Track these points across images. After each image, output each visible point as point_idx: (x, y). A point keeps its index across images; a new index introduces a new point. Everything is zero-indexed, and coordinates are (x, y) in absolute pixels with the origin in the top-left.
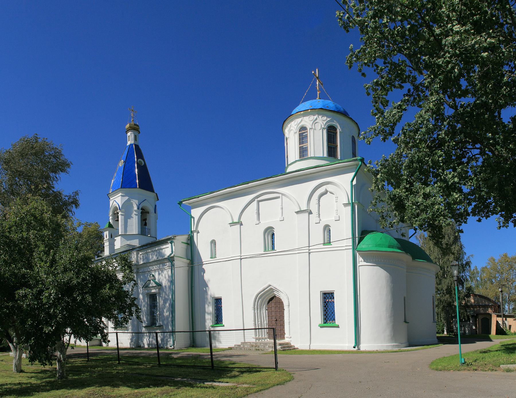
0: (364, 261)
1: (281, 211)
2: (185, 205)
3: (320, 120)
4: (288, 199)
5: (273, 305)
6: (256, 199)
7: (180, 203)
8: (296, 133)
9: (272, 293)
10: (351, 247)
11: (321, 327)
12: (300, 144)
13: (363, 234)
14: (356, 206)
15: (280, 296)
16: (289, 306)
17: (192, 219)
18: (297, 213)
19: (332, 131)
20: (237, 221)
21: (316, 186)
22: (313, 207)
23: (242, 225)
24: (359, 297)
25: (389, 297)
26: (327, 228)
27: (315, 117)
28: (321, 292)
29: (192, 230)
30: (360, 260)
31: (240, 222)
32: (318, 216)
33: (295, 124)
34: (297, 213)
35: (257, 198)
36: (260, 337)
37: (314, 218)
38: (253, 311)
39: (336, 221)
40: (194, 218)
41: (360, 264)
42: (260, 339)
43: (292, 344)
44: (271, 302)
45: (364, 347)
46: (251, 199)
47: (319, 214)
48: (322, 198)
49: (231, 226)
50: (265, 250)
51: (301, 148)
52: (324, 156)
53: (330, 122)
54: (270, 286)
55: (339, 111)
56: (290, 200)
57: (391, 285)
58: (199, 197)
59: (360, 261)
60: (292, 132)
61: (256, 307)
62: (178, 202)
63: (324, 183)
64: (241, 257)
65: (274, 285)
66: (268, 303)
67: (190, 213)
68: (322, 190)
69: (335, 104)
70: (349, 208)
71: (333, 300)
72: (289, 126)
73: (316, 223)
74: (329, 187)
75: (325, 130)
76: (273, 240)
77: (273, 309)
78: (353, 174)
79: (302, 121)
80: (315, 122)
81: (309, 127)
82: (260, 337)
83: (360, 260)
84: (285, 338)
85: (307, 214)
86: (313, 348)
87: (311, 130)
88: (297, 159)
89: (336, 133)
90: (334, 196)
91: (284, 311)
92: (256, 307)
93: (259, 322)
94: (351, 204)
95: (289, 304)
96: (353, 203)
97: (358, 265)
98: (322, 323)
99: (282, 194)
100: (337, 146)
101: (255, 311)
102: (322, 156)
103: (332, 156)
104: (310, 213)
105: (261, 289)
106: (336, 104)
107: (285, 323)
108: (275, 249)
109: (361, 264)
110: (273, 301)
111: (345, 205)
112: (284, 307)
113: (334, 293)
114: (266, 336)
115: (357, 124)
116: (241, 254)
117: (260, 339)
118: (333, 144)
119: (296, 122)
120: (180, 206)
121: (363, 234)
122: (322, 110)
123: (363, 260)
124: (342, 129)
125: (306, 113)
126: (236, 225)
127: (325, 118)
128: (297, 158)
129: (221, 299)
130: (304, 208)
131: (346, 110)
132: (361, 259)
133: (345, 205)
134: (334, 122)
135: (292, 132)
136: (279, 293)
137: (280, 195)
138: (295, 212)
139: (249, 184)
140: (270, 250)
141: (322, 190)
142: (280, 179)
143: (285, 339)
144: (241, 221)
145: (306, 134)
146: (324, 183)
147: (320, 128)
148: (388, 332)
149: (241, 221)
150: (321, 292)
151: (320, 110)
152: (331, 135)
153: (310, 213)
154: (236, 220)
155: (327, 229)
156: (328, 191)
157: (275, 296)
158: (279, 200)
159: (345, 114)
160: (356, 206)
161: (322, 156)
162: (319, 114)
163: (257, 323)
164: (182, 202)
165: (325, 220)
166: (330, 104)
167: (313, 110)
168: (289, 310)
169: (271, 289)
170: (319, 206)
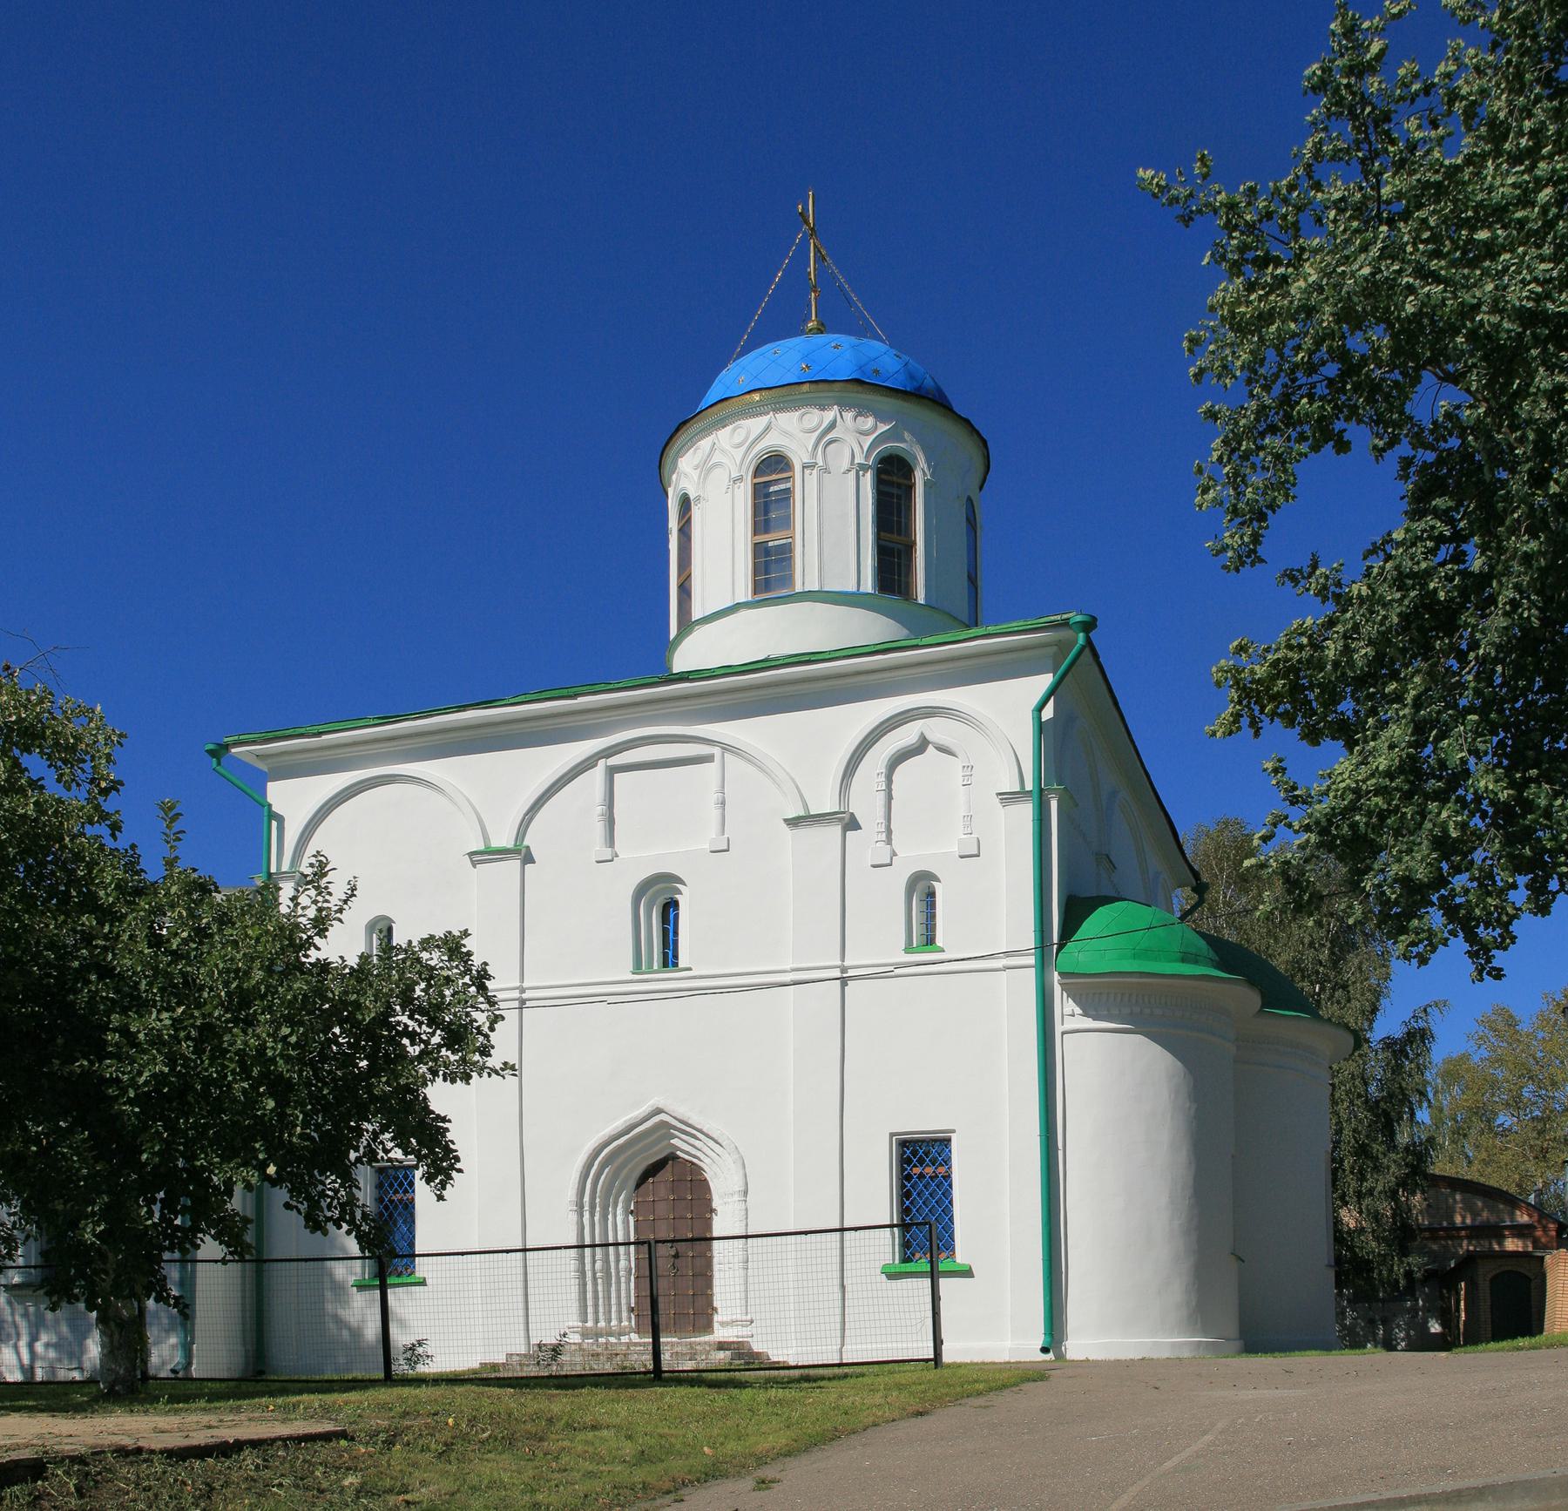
0: (1086, 1014)
1: (715, 813)
2: (238, 762)
3: (847, 429)
4: (751, 768)
5: (662, 1191)
6: (602, 762)
7: (220, 751)
8: (740, 479)
9: (664, 1143)
10: (1031, 960)
11: (892, 1276)
12: (755, 532)
13: (1076, 911)
14: (1054, 804)
15: (698, 1154)
16: (746, 1193)
17: (274, 824)
18: (793, 822)
19: (895, 479)
20: (510, 845)
21: (882, 723)
22: (865, 800)
23: (534, 862)
24: (1060, 1153)
25: (1183, 1156)
26: (921, 886)
27: (830, 415)
28: (892, 1135)
29: (273, 870)
30: (1067, 1010)
31: (524, 850)
32: (884, 837)
33: (738, 439)
34: (793, 822)
35: (608, 757)
36: (602, 1324)
37: (865, 845)
38: (574, 1217)
39: (962, 857)
40: (280, 820)
41: (1067, 1027)
42: (598, 1335)
43: (756, 1348)
44: (651, 1180)
45: (1078, 1346)
46: (579, 760)
47: (889, 832)
48: (901, 769)
49: (474, 864)
50: (637, 967)
51: (760, 551)
52: (862, 590)
53: (885, 442)
54: (659, 1111)
55: (919, 388)
56: (763, 770)
57: (1190, 1108)
58: (320, 734)
59: (1067, 1012)
60: (720, 478)
61: (586, 1199)
62: (210, 747)
63: (911, 714)
64: (523, 991)
65: (681, 1108)
66: (638, 1186)
67: (264, 794)
68: (905, 736)
69: (904, 356)
70: (1026, 811)
71: (942, 1170)
72: (705, 444)
73: (874, 866)
74: (935, 729)
75: (869, 475)
76: (671, 928)
77: (662, 1209)
78: (1045, 681)
79: (768, 428)
80: (826, 439)
81: (798, 457)
82: (602, 1324)
83: (1067, 1010)
84: (716, 1325)
85: (836, 830)
86: (856, 1352)
87: (807, 472)
88: (743, 600)
89: (910, 488)
90: (956, 764)
91: (710, 1219)
92: (586, 1199)
93: (598, 1265)
94: (1036, 795)
95: (747, 1184)
96: (1041, 790)
97: (1059, 1029)
98: (894, 1260)
99: (726, 748)
100: (911, 546)
101: (581, 1215)
102: (852, 587)
103: (892, 592)
104: (852, 824)
105: (618, 1124)
106: (906, 358)
107: (716, 1267)
108: (681, 965)
109: (1071, 1024)
110: (666, 1174)
111: (1007, 798)
112: (710, 1200)
113: (949, 1140)
114: (625, 1323)
115: (985, 443)
116: (522, 980)
117: (598, 1335)
118: (899, 534)
119: (739, 436)
120: (219, 764)
121: (1076, 911)
122: (860, 388)
123: (1078, 1010)
124: (935, 467)
125: (785, 395)
126: (501, 859)
127: (869, 422)
128: (744, 592)
129: (946, 1142)
130: (826, 802)
131: (943, 388)
132: (1071, 1006)
133: (1007, 798)
134: (904, 441)
135: (720, 478)
136: (697, 1143)
137: (716, 751)
138: (785, 820)
139: (580, 700)
140: (655, 967)
141: (905, 736)
142: (721, 687)
143: (712, 1332)
144: (526, 843)
145: (782, 486)
146: (915, 712)
147: (846, 464)
148: (1176, 1293)
149: (526, 843)
150: (892, 1135)
151: (850, 386)
152: (891, 495)
153: (852, 824)
154: (504, 840)
155: (923, 890)
156: (929, 743)
157: (671, 1158)
158: (711, 769)
159: (936, 400)
160: (1054, 804)
161: (855, 589)
162: (844, 405)
163: (588, 1267)
164: (227, 747)
165: (912, 856)
166: (882, 356)
167: (821, 386)
168: (747, 1210)
169: (664, 1124)
170: (890, 798)
